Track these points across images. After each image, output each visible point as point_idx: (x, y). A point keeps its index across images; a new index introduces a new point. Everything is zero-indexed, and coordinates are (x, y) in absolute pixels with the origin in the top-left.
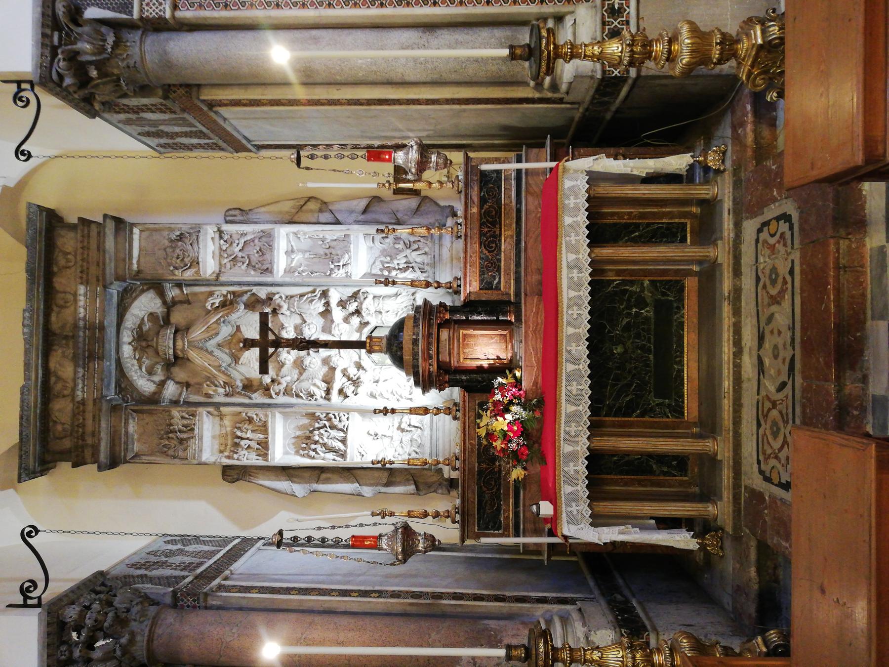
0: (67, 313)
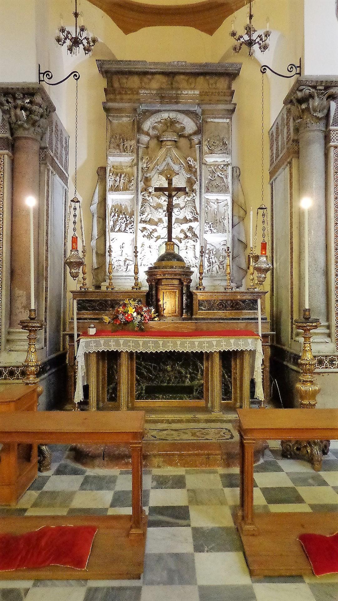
0: (184, 84)
